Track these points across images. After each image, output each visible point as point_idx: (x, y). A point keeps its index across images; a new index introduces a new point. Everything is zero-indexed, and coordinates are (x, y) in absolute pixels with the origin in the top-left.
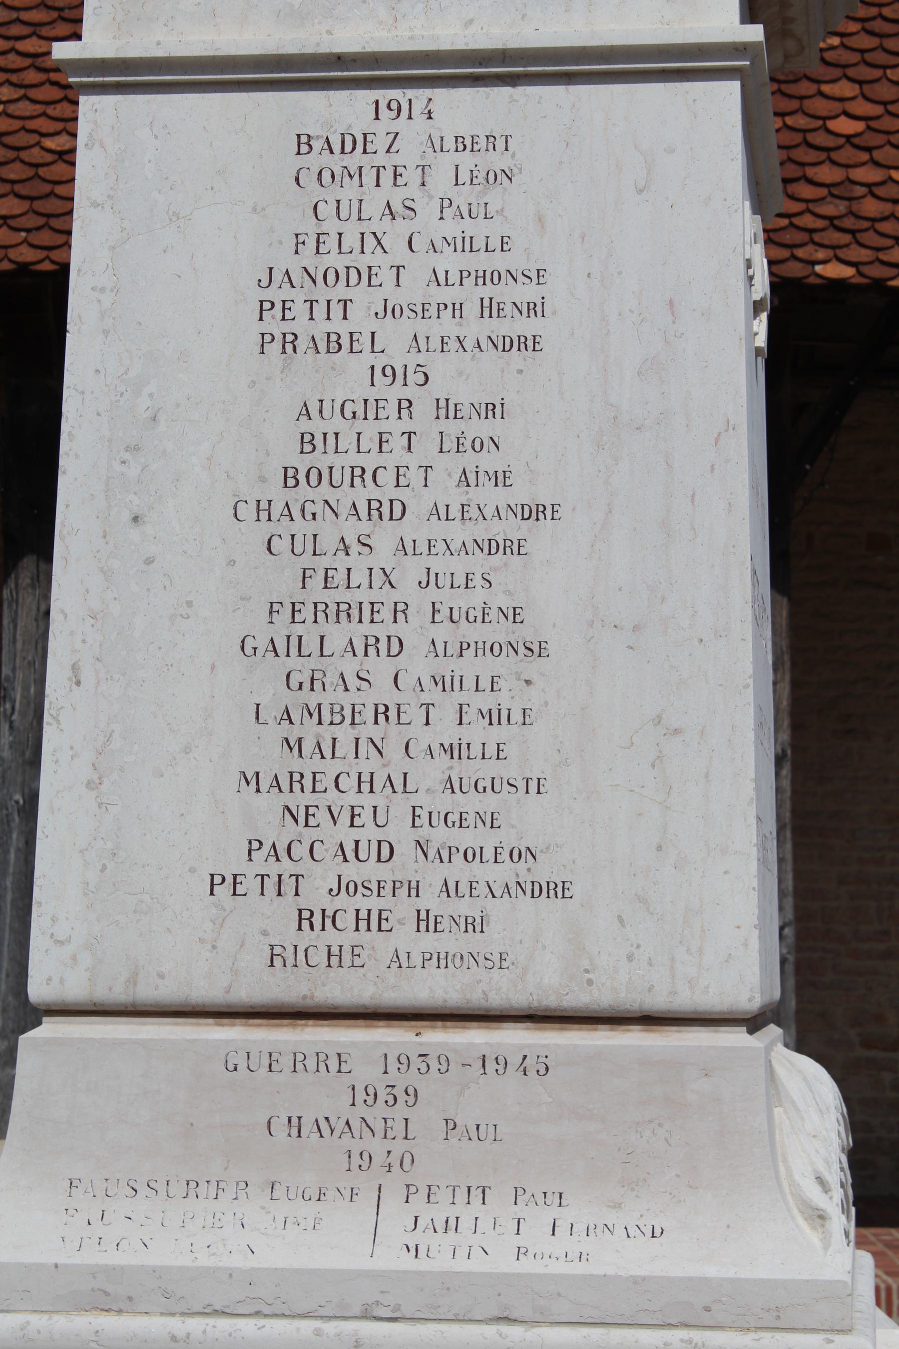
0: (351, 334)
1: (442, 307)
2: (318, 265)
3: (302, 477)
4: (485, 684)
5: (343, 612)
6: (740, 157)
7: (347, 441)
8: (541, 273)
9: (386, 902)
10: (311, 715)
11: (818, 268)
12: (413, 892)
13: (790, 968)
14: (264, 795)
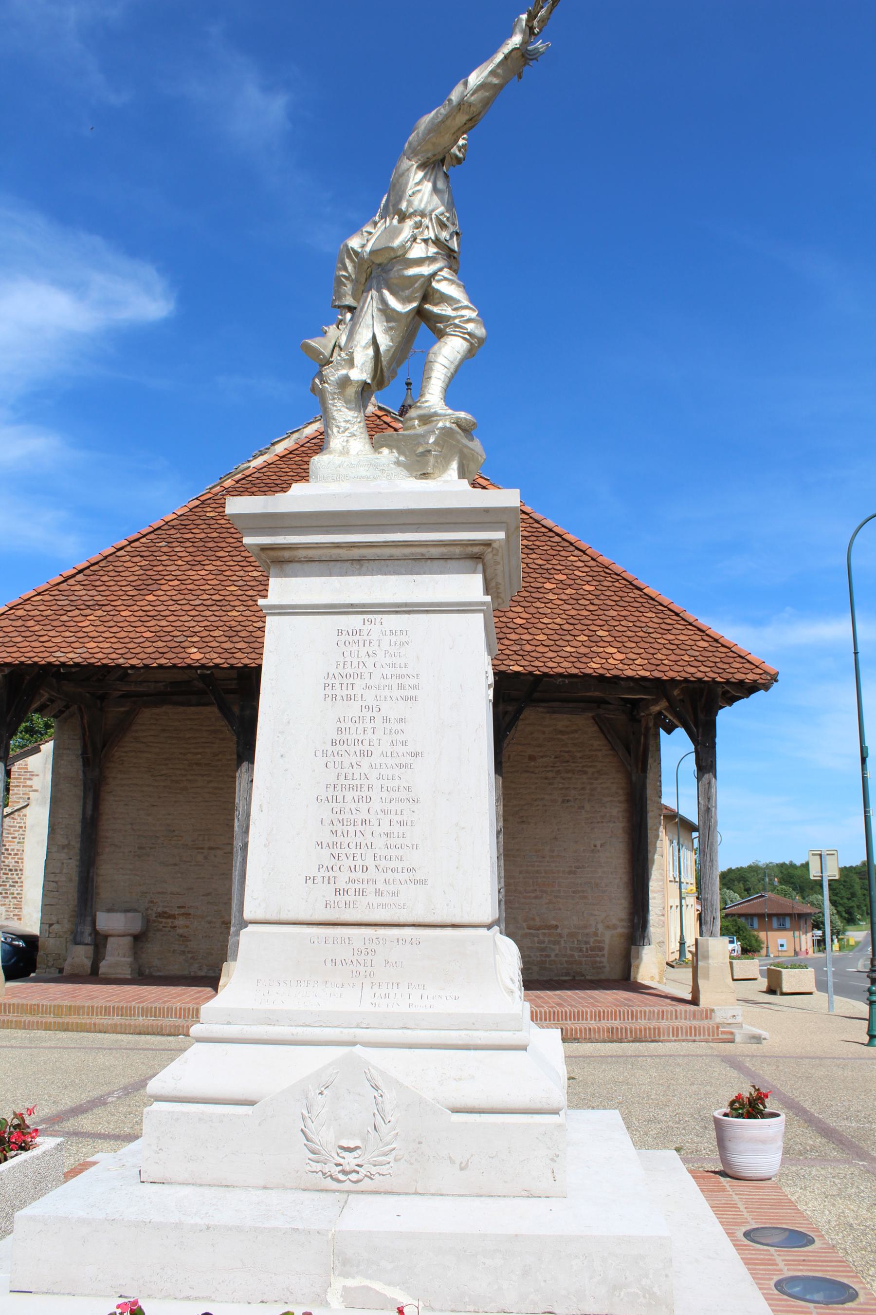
3: (338, 742)
5: (351, 788)
7: (353, 731)
9: (365, 886)
13: (503, 903)
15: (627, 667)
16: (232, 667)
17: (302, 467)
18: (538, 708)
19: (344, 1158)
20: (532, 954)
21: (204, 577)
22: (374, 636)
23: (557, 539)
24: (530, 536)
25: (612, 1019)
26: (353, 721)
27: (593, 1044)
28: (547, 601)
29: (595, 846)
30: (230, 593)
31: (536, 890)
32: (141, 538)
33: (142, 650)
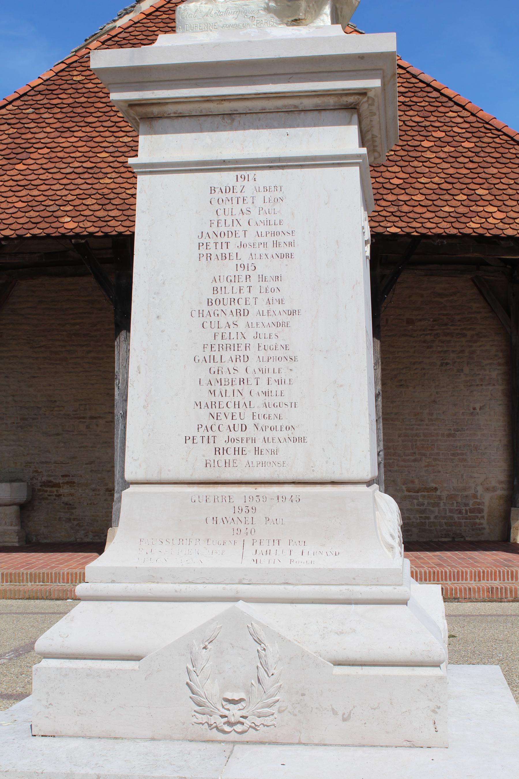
0: (230, 254)
1: (260, 244)
2: (218, 231)
3: (214, 302)
4: (276, 371)
5: (228, 347)
6: (359, 192)
7: (229, 290)
8: (293, 232)
9: (244, 445)
10: (218, 382)
11: (388, 229)
12: (253, 441)
13: (382, 465)
14: (202, 409)
15: (507, 226)
16: (106, 235)
17: (169, 25)
18: (416, 271)
19: (228, 710)
20: (412, 516)
21: (74, 144)
22: (248, 193)
23: (435, 94)
24: (407, 92)
25: (492, 580)
26: (229, 281)
27: (473, 603)
28: (425, 160)
29: (474, 409)
30: (101, 160)
31: (415, 453)
32: (7, 105)
33: (15, 220)
